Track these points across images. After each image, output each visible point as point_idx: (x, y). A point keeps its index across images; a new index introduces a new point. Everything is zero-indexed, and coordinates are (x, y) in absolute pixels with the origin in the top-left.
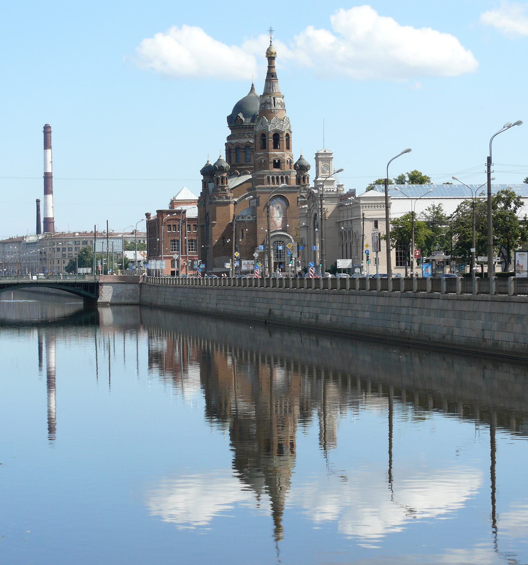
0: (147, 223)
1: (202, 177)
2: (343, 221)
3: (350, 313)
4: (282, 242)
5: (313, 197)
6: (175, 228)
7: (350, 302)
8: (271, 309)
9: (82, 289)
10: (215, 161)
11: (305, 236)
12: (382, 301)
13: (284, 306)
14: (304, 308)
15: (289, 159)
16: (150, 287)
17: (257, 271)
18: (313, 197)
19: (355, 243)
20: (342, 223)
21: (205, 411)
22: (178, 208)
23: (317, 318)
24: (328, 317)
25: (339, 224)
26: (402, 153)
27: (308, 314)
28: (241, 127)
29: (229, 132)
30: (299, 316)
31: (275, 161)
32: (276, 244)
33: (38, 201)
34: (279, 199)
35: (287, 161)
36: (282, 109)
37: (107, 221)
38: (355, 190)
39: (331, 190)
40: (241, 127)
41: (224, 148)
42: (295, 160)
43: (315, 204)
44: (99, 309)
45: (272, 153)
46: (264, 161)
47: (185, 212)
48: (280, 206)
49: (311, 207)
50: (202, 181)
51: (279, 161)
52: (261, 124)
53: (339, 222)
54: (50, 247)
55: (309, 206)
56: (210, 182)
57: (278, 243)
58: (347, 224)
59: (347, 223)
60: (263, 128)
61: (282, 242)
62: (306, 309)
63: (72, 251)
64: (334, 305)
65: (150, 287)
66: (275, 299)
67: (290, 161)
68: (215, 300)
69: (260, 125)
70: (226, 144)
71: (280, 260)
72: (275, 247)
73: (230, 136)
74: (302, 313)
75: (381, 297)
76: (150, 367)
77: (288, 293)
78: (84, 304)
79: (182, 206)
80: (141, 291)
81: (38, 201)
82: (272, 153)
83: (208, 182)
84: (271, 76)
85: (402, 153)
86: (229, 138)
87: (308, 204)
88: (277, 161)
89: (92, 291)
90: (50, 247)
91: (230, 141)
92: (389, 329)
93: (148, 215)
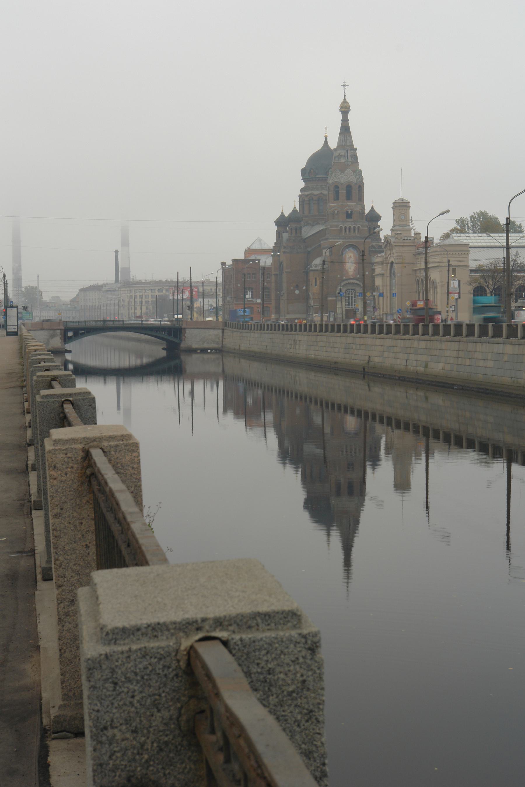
0: (222, 272)
1: (276, 228)
2: (420, 269)
3: (468, 362)
4: (354, 290)
5: (390, 245)
6: (250, 276)
7: (468, 350)
8: (369, 356)
9: (167, 334)
10: (290, 211)
11: (381, 284)
12: (509, 349)
13: (386, 354)
14: (411, 355)
15: (362, 210)
16: (233, 333)
17: (400, 315)
18: (390, 245)
19: (433, 291)
20: (419, 270)
21: (365, 505)
22: (253, 257)
23: (426, 366)
24: (440, 366)
25: (416, 272)
26: (439, 215)
27: (415, 362)
28: (314, 179)
29: (302, 184)
30: (404, 362)
31: (347, 212)
32: (348, 292)
33: (117, 252)
34: (351, 249)
35: (360, 212)
36: (354, 161)
37: (178, 272)
38: (433, 239)
39: (408, 239)
40: (314, 179)
41: (298, 199)
42: (367, 211)
43: (392, 253)
44: (183, 357)
45: (345, 204)
46: (338, 212)
47: (259, 260)
48: (352, 255)
49: (387, 256)
50: (276, 231)
51: (351, 212)
52: (335, 176)
53: (416, 270)
54: (128, 294)
55: (386, 254)
56: (284, 232)
57: (350, 291)
58: (420, 272)
59: (420, 271)
60: (336, 180)
61: (354, 290)
62: (412, 357)
63: (148, 298)
64: (448, 353)
65: (233, 333)
66: (375, 345)
67: (362, 212)
68: (305, 346)
69: (333, 177)
70: (300, 196)
71: (352, 307)
72: (347, 295)
73: (304, 187)
74: (408, 361)
75: (508, 345)
76: (225, 411)
77: (391, 340)
78: (167, 353)
79: (256, 256)
80: (223, 336)
81: (117, 252)
82: (345, 204)
83: (282, 232)
84: (345, 130)
85: (439, 215)
86: (302, 190)
87: (385, 252)
88: (349, 212)
89: (176, 336)
90: (128, 294)
91: (303, 193)
92: (519, 380)
93: (223, 264)
